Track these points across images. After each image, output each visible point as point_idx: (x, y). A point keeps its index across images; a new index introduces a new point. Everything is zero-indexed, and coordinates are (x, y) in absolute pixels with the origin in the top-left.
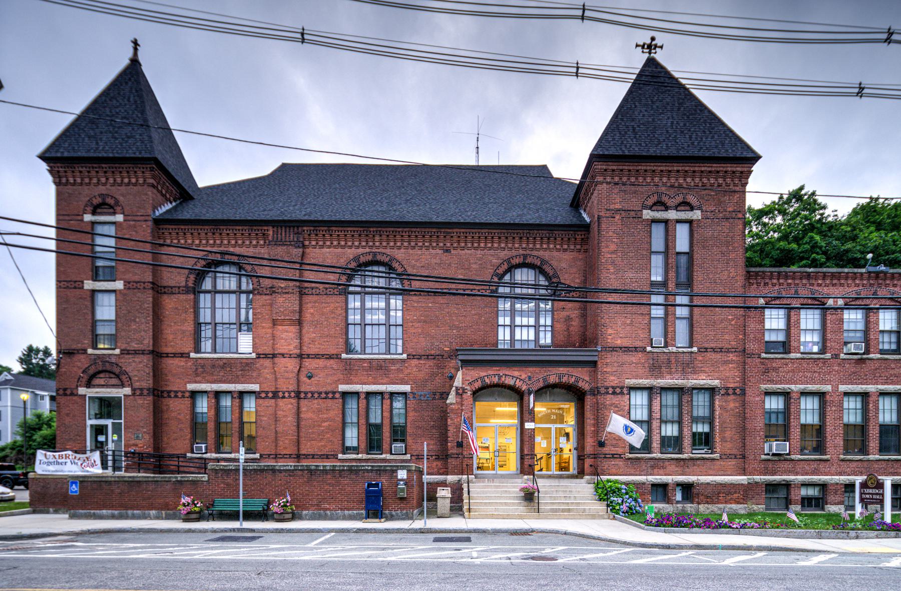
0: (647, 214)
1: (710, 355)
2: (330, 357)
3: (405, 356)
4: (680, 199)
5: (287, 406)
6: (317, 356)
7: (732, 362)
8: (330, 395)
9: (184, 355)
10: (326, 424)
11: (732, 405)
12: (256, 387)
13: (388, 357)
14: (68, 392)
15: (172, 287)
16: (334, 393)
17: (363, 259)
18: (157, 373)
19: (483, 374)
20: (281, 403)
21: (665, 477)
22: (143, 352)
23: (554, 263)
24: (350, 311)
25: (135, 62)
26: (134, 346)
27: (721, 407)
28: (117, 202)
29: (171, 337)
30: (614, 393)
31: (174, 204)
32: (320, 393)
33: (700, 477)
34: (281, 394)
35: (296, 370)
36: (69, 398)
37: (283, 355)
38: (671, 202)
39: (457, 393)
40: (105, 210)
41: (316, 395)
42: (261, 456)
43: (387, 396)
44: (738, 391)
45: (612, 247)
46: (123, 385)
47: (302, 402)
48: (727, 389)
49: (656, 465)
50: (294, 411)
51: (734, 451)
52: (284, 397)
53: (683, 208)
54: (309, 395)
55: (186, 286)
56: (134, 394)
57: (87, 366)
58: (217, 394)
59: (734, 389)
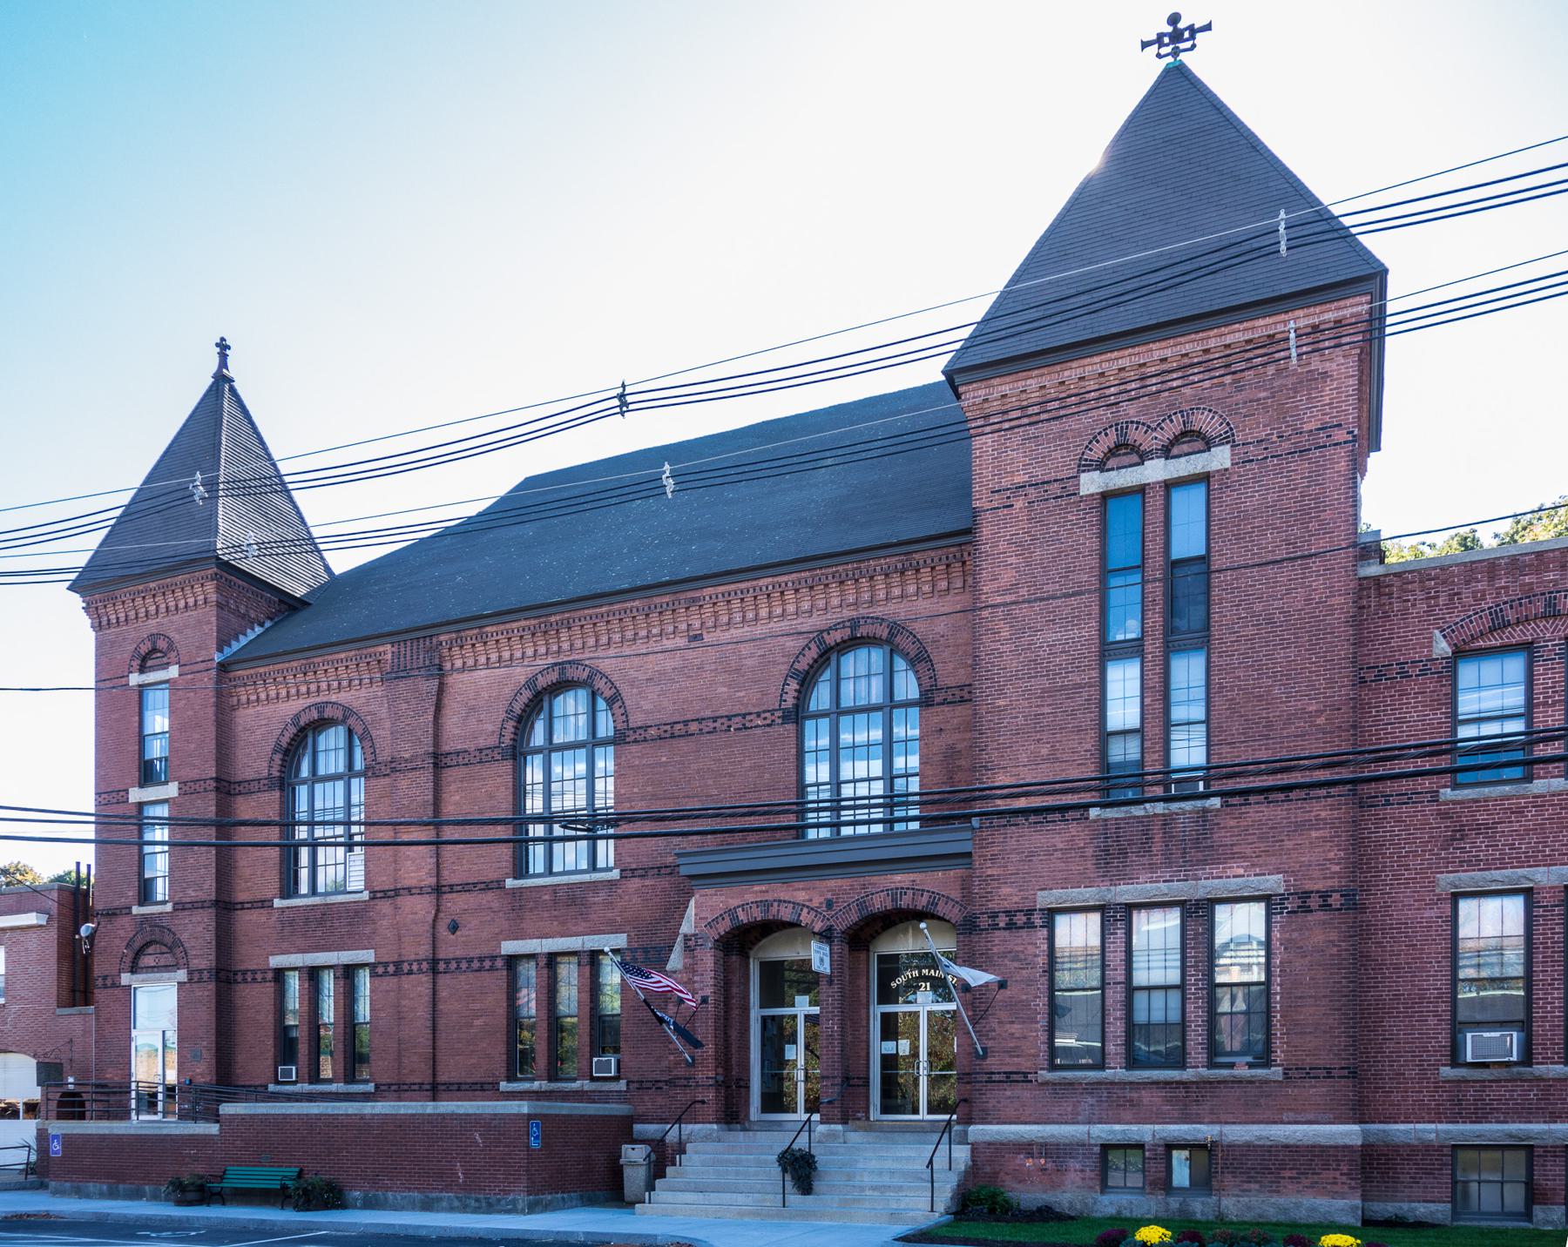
0: (1091, 483)
1: (1258, 812)
2: (487, 886)
3: (615, 874)
4: (1172, 428)
6: (466, 888)
7: (1317, 823)
8: (487, 964)
9: (265, 904)
10: (477, 1022)
11: (1318, 938)
12: (368, 956)
14: (109, 982)
15: (249, 782)
16: (493, 958)
17: (542, 682)
19: (734, 902)
21: (1134, 1128)
23: (919, 628)
24: (842, 752)
25: (222, 380)
28: (171, 646)
29: (248, 871)
30: (1011, 926)
31: (258, 630)
33: (1227, 1129)
34: (406, 967)
35: (430, 918)
36: (110, 991)
38: (1148, 441)
39: (687, 948)
41: (464, 965)
42: (377, 1087)
45: (1007, 577)
48: (1306, 895)
49: (1117, 1100)
50: (427, 999)
51: (1325, 1060)
52: (410, 972)
53: (1185, 448)
54: (453, 965)
55: (270, 777)
56: (190, 980)
58: (552, 959)
59: (1325, 895)
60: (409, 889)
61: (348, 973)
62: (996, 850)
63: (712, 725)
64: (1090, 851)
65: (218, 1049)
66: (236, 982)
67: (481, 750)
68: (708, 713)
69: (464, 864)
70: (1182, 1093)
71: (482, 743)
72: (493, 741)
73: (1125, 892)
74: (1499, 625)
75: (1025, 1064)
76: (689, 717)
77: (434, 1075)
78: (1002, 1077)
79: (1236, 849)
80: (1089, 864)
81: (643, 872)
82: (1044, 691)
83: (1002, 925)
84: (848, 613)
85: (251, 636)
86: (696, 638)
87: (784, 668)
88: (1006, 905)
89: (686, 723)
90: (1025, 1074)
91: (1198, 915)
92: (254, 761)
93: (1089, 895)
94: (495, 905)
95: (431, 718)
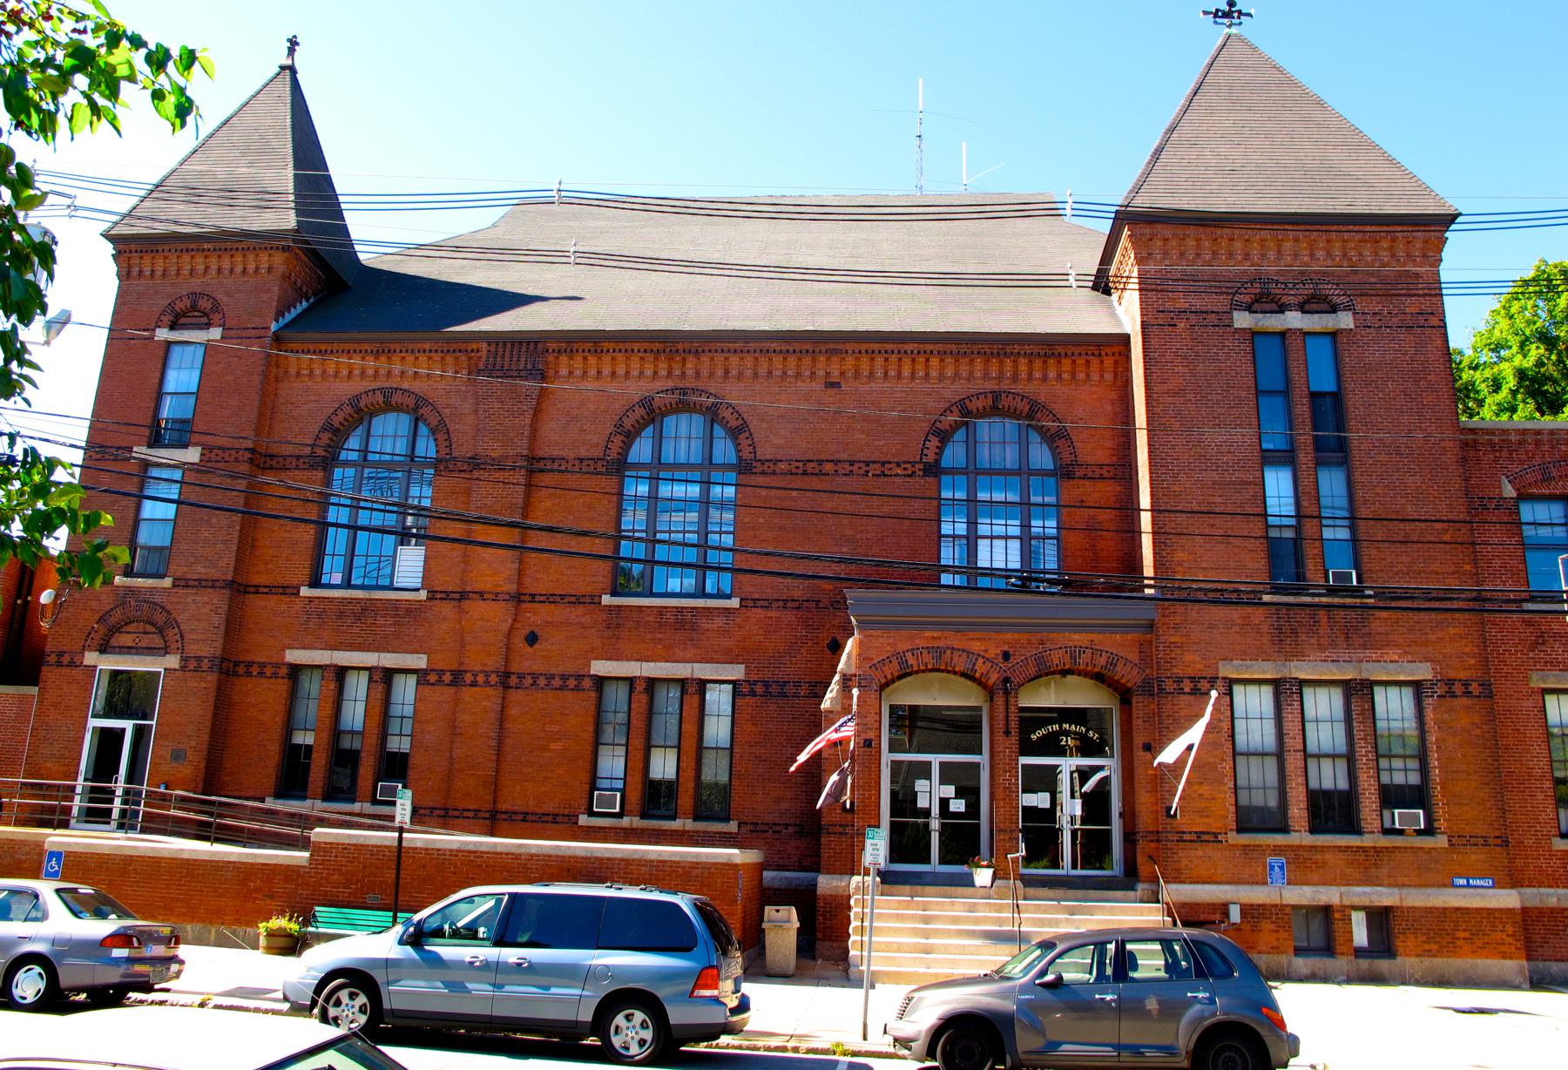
2: (578, 600)
3: (734, 603)
5: (480, 703)
6: (551, 599)
8: (572, 683)
10: (552, 746)
13: (700, 603)
14: (66, 659)
16: (580, 677)
18: (234, 626)
19: (902, 647)
20: (467, 694)
22: (213, 584)
23: (1058, 408)
26: (200, 570)
27: (1441, 725)
28: (216, 307)
32: (551, 677)
34: (468, 678)
35: (505, 627)
36: (64, 670)
37: (481, 595)
40: (193, 320)
41: (542, 682)
43: (640, 687)
44: (1474, 688)
46: (165, 651)
47: (515, 696)
48: (1450, 682)
52: (474, 684)
53: (1315, 307)
54: (528, 681)
55: (312, 455)
56: (183, 668)
57: (108, 608)
59: (1466, 684)
60: (481, 594)
61: (386, 677)
62: (1178, 619)
63: (1098, 472)
64: (1265, 628)
65: (209, 753)
66: (236, 674)
67: (581, 460)
68: (844, 456)
69: (548, 575)
70: (1361, 857)
71: (583, 453)
72: (598, 452)
73: (1301, 670)
74: (1547, 479)
75: (1215, 826)
76: (823, 457)
77: (495, 802)
78: (1194, 837)
79: (1390, 637)
80: (1266, 640)
81: (768, 604)
82: (1214, 483)
83: (1187, 690)
84: (991, 386)
85: (299, 309)
86: (834, 385)
87: (926, 426)
88: (1190, 672)
89: (820, 462)
90: (1215, 835)
91: (1358, 693)
93: (1269, 670)
94: (586, 620)
95: (528, 421)
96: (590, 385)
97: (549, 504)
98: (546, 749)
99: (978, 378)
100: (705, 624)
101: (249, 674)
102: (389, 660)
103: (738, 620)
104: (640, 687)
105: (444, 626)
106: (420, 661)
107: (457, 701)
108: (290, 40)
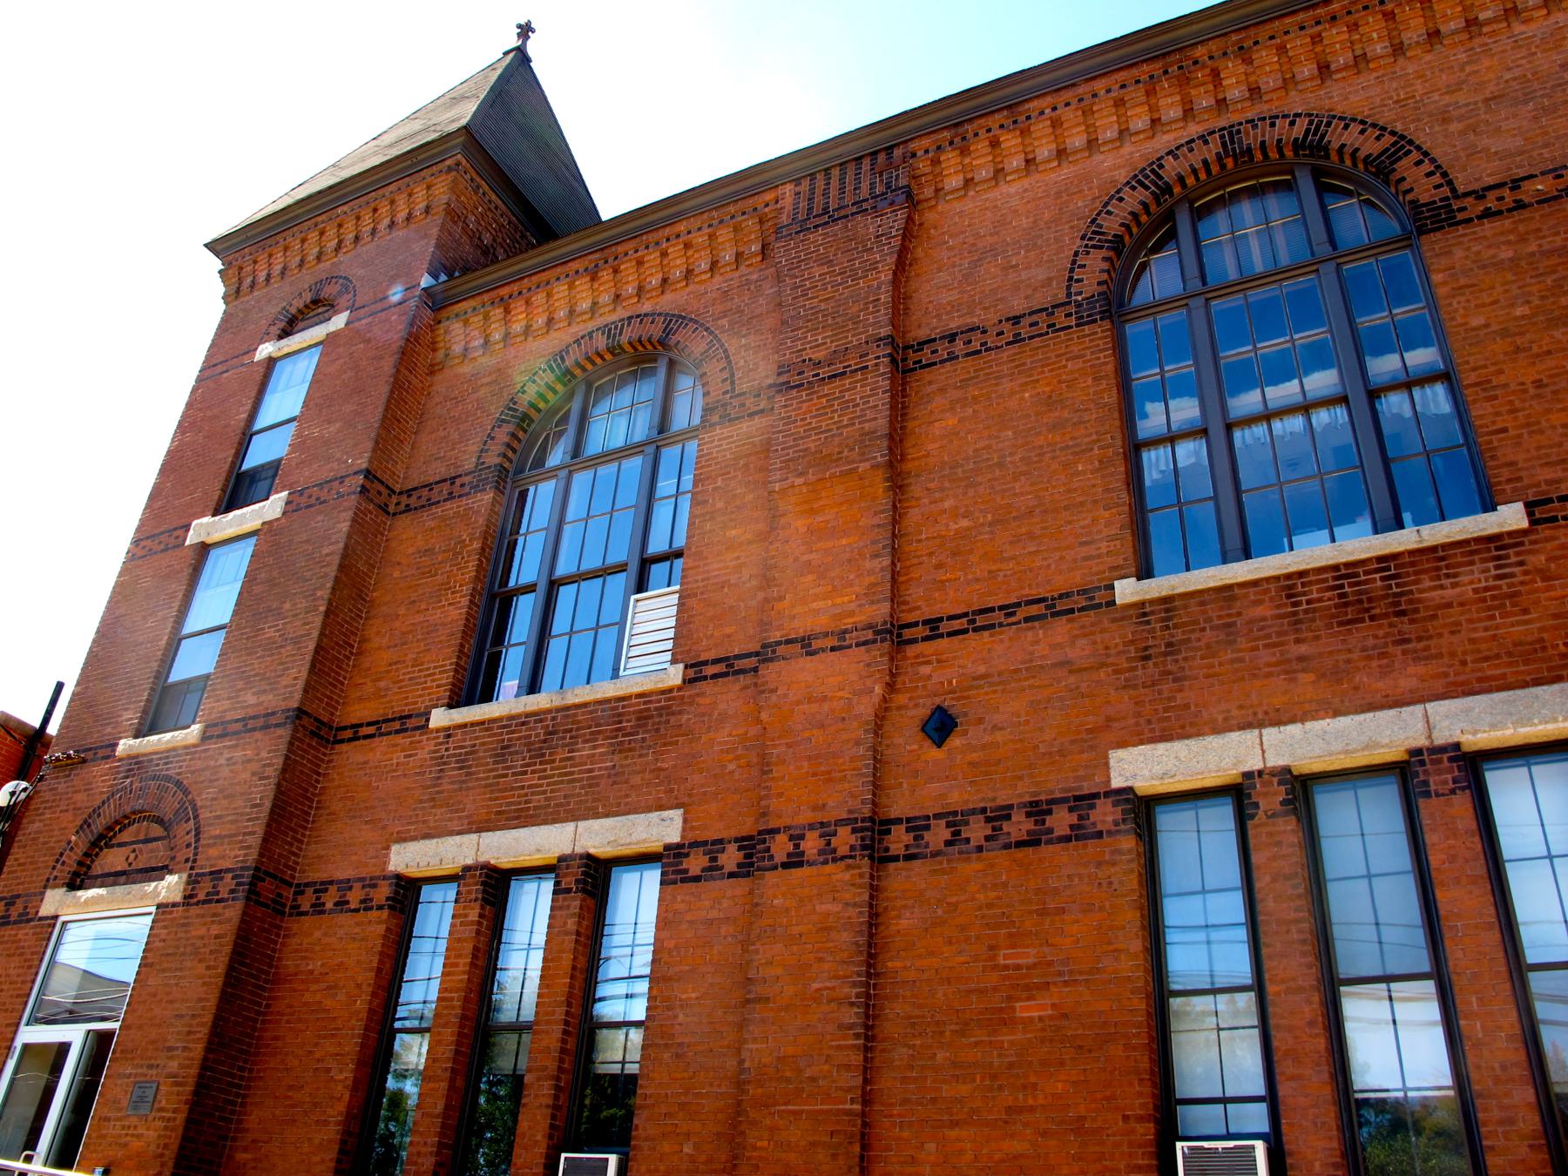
2: (1052, 608)
6: (976, 621)
8: (1061, 820)
10: (1026, 1010)
15: (429, 486)
16: (1082, 802)
20: (777, 887)
25: (520, 60)
32: (998, 816)
34: (781, 847)
35: (866, 708)
37: (806, 644)
41: (976, 831)
43: (1270, 799)
47: (900, 879)
52: (795, 861)
54: (938, 834)
56: (188, 898)
67: (1016, 320)
71: (1018, 305)
92: (461, 444)
94: (1080, 651)
95: (886, 276)
96: (1012, 191)
97: (952, 421)
98: (1002, 1020)
99: (1121, 150)
100: (1429, 591)
101: (318, 908)
102: (597, 836)
103: (1538, 560)
104: (1270, 799)
105: (722, 736)
106: (664, 828)
107: (754, 908)
108: (519, 26)
